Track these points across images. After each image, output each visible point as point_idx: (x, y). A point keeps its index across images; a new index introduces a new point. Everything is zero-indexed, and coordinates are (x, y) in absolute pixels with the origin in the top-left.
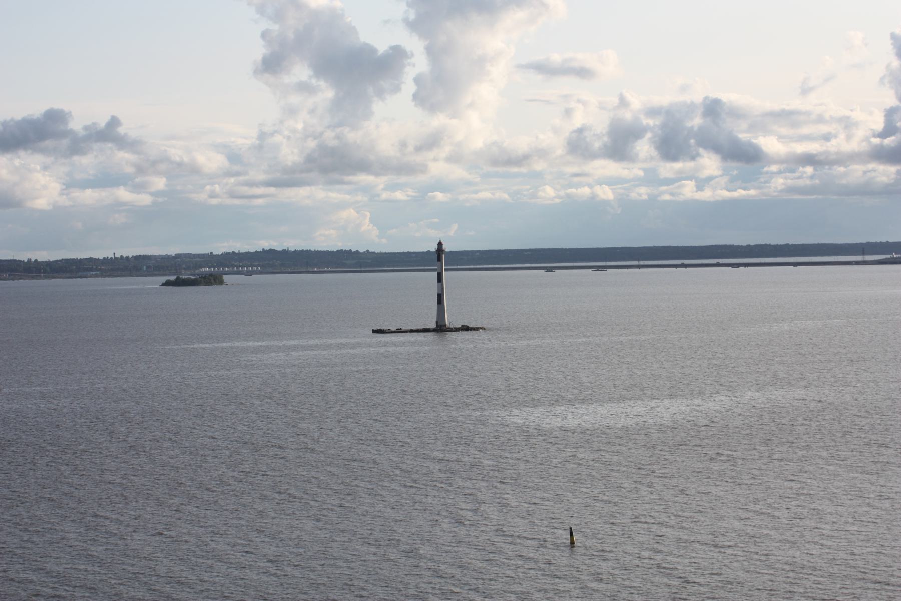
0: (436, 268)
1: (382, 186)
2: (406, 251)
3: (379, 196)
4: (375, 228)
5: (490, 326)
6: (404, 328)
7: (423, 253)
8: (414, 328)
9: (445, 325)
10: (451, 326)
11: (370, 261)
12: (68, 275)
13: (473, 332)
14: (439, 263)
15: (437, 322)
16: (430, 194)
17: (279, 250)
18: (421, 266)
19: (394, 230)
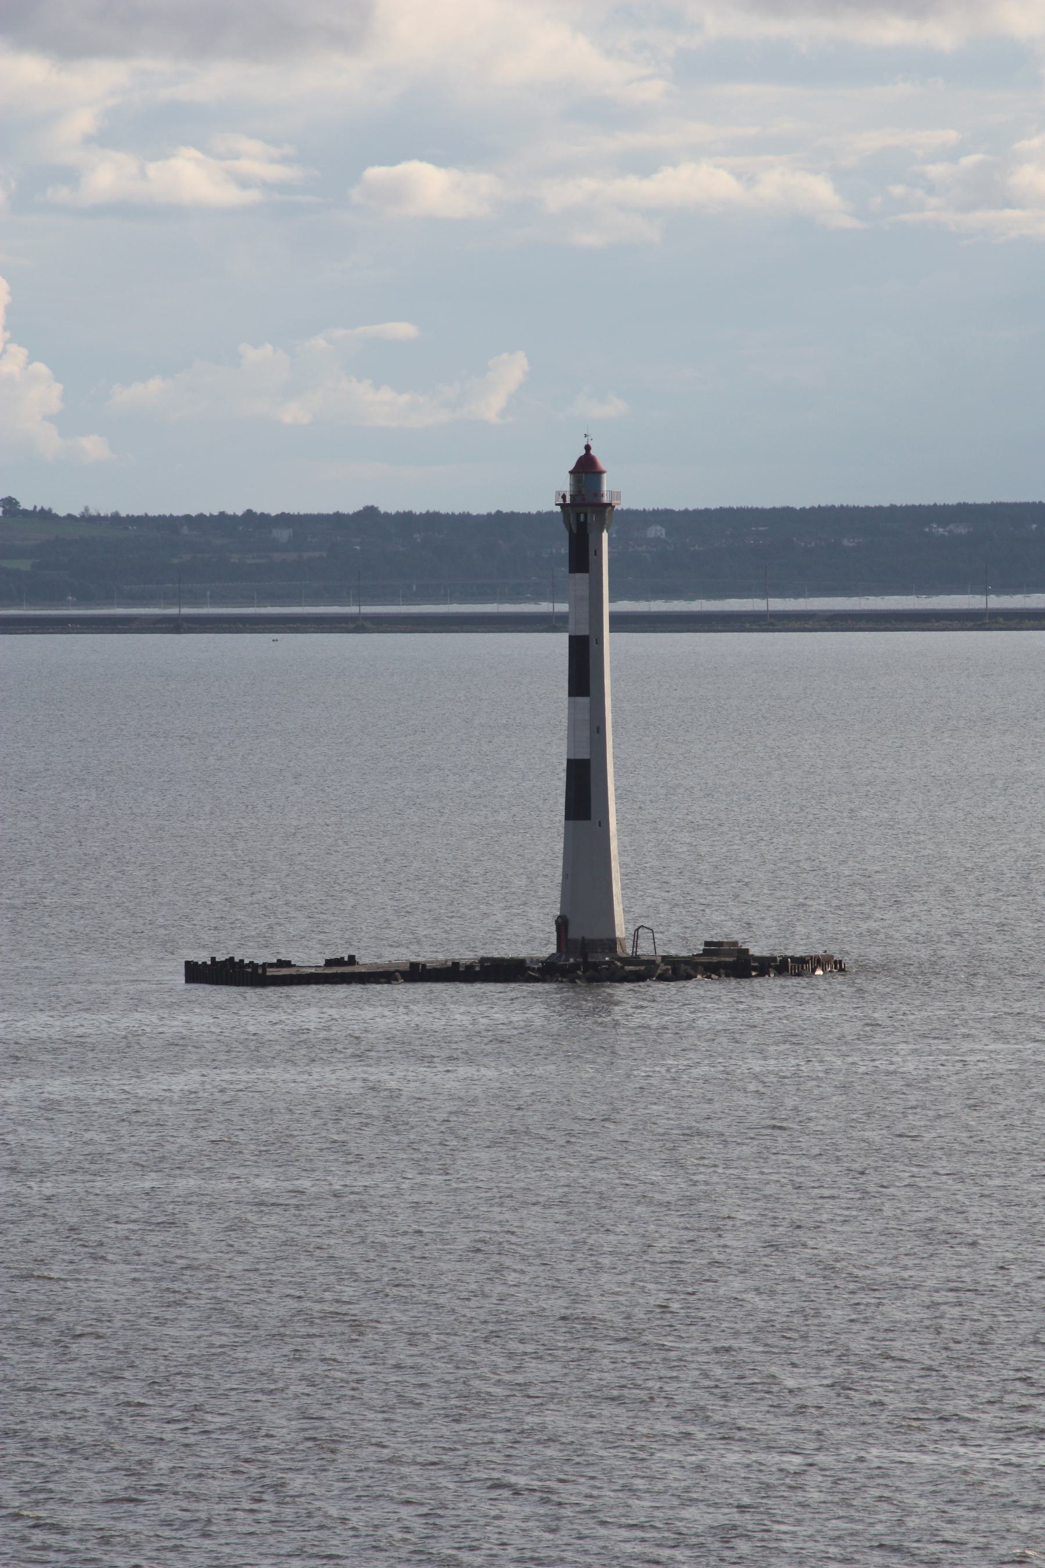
0: (563, 608)
1: (84, 121)
2: (236, 509)
3: (70, 176)
4: (40, 368)
5: (875, 954)
6: (367, 959)
7: (338, 519)
8: (430, 955)
9: (611, 943)
10: (645, 949)
11: (24, 565)
12: (970, 624)
13: (771, 985)
14: (582, 578)
15: (562, 925)
16: (376, 173)
17: (677, 509)
18: (537, 598)
19: (155, 384)
